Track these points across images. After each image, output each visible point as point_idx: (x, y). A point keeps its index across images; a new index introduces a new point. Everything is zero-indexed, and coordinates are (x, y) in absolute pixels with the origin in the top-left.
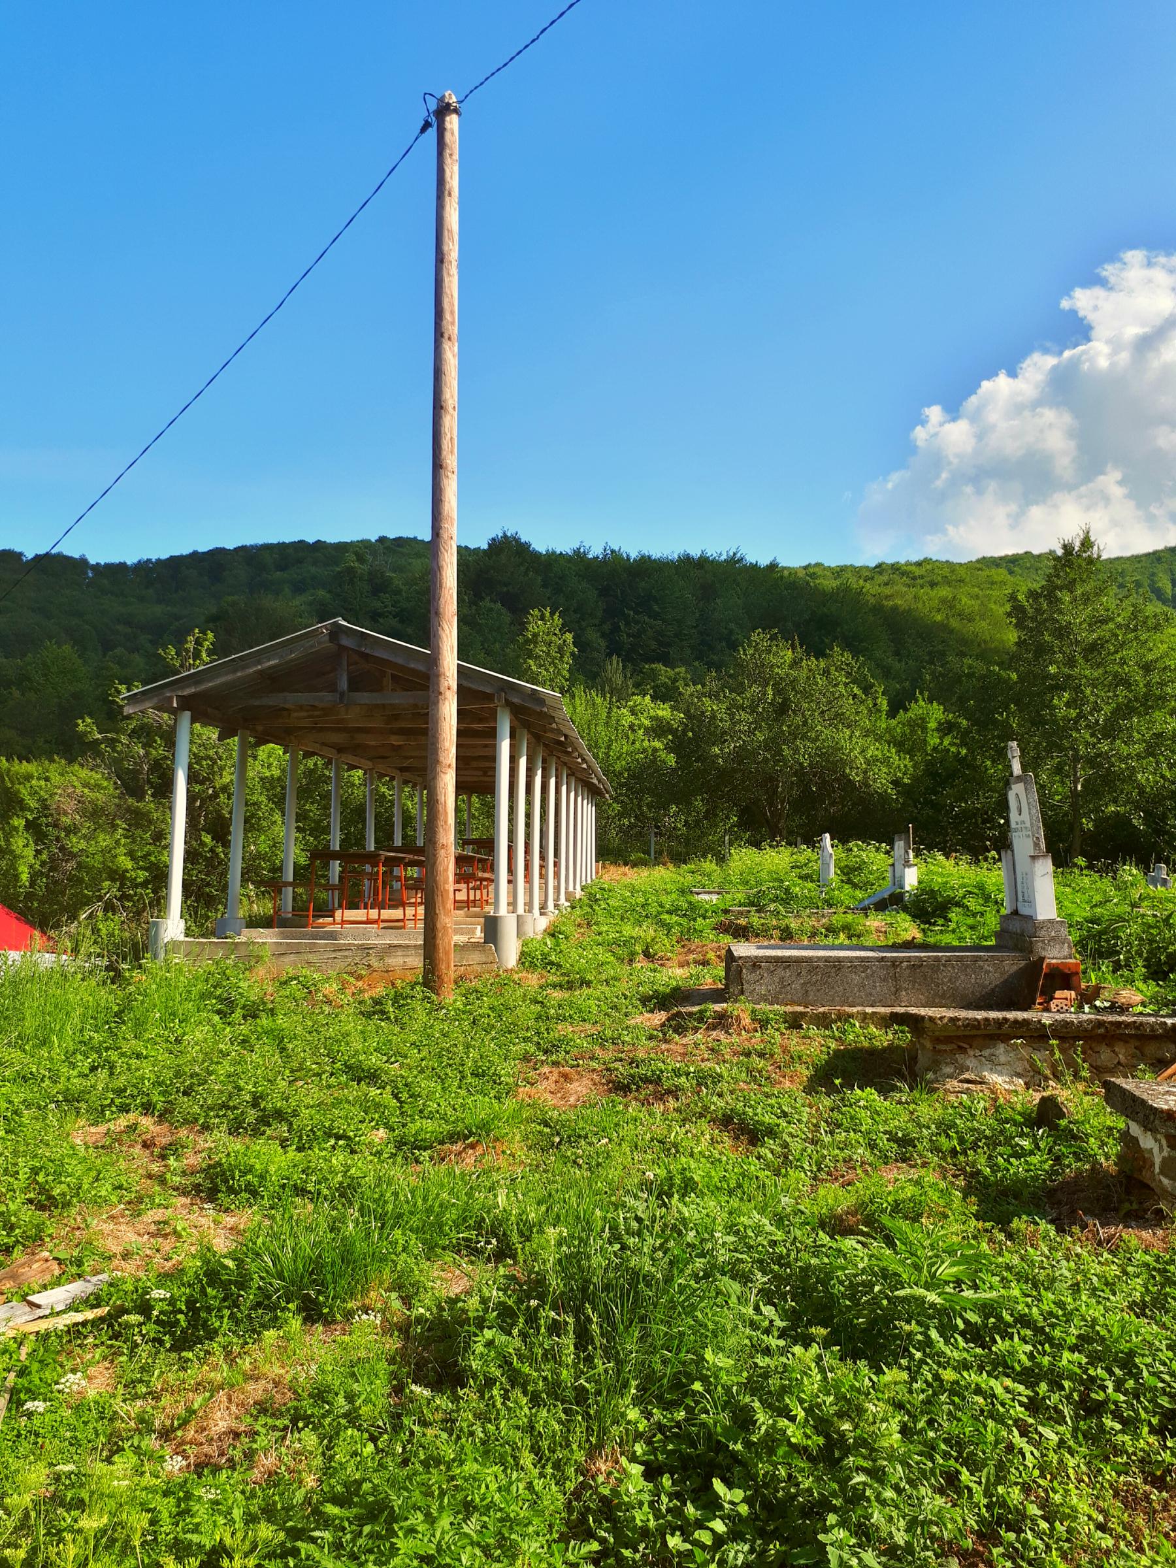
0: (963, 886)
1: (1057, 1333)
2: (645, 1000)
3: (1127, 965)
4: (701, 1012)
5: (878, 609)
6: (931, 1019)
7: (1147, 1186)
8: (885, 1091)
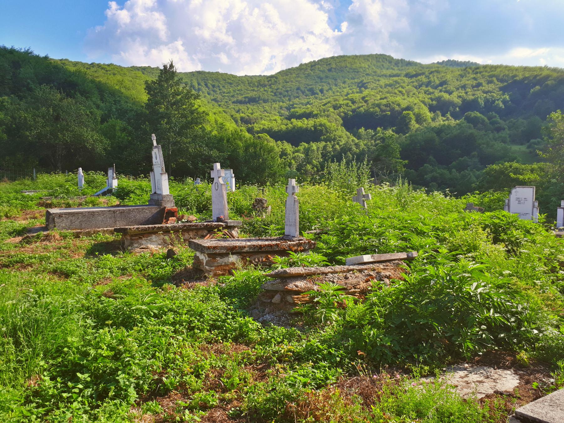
0: (134, 186)
1: (180, 311)
2: (10, 234)
3: (191, 209)
4: (38, 235)
5: (93, 82)
6: (130, 229)
7: (202, 270)
8: (114, 254)
